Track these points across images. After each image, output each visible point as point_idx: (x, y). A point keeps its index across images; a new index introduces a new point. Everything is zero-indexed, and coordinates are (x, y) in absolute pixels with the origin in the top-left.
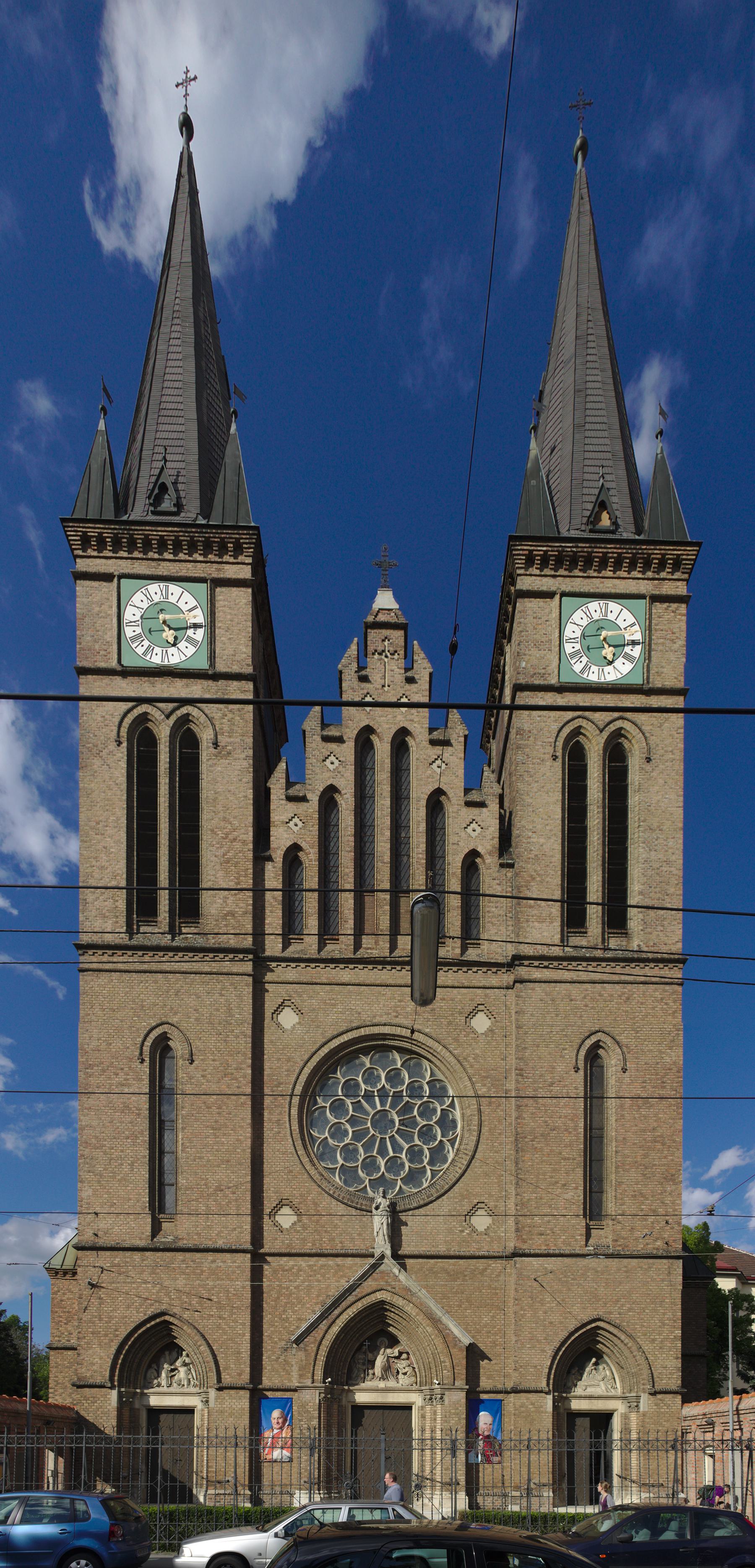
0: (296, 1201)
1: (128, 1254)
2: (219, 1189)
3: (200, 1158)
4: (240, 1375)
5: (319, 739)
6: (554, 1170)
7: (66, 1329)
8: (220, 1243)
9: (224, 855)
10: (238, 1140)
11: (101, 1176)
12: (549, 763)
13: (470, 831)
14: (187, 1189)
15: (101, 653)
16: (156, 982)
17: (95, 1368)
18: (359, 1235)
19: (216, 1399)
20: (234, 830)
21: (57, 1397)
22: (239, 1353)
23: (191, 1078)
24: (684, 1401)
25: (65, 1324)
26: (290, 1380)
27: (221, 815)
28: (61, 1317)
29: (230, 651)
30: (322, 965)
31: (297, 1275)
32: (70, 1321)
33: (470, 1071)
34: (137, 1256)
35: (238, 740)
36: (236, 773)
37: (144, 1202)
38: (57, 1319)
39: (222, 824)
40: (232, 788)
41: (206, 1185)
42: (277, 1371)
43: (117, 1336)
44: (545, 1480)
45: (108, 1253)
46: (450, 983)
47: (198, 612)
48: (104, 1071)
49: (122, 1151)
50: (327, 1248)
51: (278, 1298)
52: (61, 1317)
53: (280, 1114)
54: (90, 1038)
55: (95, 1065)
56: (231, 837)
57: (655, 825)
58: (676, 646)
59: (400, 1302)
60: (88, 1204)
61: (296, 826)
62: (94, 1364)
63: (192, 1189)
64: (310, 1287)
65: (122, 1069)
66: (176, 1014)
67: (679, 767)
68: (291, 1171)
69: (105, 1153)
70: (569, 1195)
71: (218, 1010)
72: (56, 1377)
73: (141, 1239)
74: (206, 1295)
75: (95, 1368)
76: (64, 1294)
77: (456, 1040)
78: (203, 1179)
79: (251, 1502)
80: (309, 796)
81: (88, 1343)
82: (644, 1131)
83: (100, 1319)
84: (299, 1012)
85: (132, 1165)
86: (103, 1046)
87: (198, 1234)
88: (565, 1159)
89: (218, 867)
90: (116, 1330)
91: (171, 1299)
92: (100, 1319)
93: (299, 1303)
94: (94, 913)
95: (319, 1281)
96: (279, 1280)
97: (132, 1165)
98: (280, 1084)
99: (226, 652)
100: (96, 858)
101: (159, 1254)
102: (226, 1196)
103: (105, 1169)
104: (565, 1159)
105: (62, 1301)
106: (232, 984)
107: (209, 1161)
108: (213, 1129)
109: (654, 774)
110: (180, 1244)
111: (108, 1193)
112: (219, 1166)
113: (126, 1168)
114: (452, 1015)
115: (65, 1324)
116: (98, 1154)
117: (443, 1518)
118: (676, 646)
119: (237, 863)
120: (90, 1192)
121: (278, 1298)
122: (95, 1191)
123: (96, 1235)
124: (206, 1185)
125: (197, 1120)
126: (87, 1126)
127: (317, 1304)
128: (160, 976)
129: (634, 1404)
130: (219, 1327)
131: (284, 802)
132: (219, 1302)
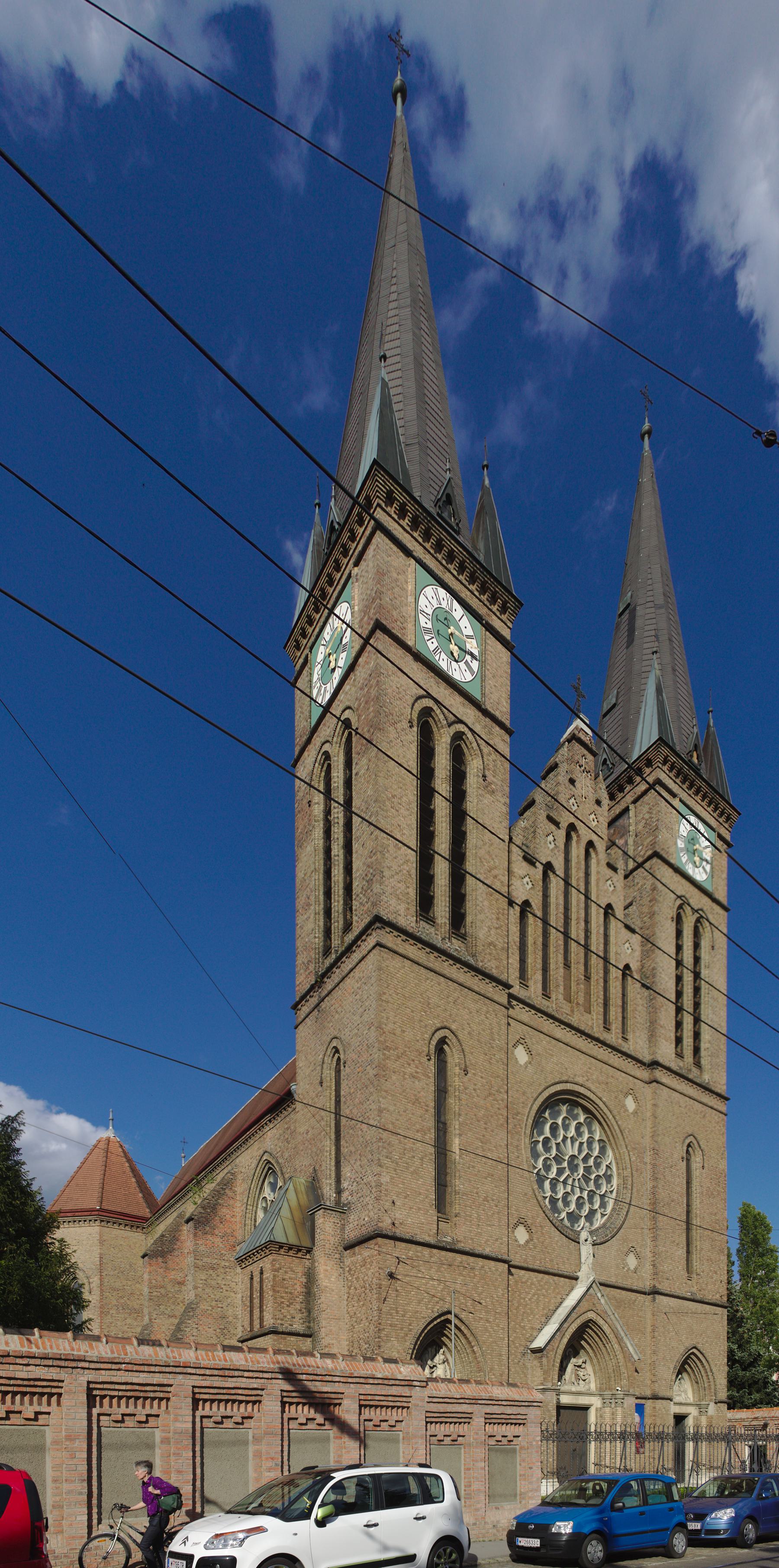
0: (529, 1222)
1: (420, 1248)
3: (473, 1167)
5: (544, 815)
7: (289, 1312)
8: (487, 1251)
11: (397, 1163)
14: (464, 1194)
15: (398, 623)
20: (496, 868)
22: (501, 1355)
23: (466, 1089)
24: (729, 1408)
25: (288, 1306)
28: (282, 1297)
30: (545, 1018)
32: (292, 1304)
34: (426, 1251)
38: (279, 1300)
39: (487, 857)
43: (410, 1330)
44: (670, 1466)
45: (403, 1245)
48: (399, 1057)
50: (549, 1267)
51: (518, 1307)
52: (282, 1297)
55: (390, 1048)
59: (601, 1322)
60: (386, 1190)
63: (466, 1194)
65: (413, 1060)
66: (454, 1021)
67: (725, 961)
68: (526, 1194)
71: (484, 1030)
73: (429, 1236)
74: (477, 1299)
76: (286, 1272)
77: (619, 1113)
78: (474, 1188)
79: (144, 1502)
83: (397, 1312)
84: (529, 1052)
85: (422, 1159)
86: (398, 1031)
87: (472, 1239)
89: (484, 896)
90: (410, 1325)
92: (397, 1312)
93: (532, 1313)
98: (519, 1113)
101: (444, 1253)
102: (491, 1207)
106: (494, 1011)
107: (479, 1171)
108: (482, 1142)
109: (715, 959)
110: (460, 1246)
111: (403, 1183)
113: (417, 1162)
115: (288, 1306)
120: (388, 1179)
121: (518, 1307)
122: (392, 1178)
123: (394, 1224)
126: (385, 1109)
128: (442, 979)
129: (702, 1409)
130: (486, 1330)
131: (521, 859)
132: (486, 1306)
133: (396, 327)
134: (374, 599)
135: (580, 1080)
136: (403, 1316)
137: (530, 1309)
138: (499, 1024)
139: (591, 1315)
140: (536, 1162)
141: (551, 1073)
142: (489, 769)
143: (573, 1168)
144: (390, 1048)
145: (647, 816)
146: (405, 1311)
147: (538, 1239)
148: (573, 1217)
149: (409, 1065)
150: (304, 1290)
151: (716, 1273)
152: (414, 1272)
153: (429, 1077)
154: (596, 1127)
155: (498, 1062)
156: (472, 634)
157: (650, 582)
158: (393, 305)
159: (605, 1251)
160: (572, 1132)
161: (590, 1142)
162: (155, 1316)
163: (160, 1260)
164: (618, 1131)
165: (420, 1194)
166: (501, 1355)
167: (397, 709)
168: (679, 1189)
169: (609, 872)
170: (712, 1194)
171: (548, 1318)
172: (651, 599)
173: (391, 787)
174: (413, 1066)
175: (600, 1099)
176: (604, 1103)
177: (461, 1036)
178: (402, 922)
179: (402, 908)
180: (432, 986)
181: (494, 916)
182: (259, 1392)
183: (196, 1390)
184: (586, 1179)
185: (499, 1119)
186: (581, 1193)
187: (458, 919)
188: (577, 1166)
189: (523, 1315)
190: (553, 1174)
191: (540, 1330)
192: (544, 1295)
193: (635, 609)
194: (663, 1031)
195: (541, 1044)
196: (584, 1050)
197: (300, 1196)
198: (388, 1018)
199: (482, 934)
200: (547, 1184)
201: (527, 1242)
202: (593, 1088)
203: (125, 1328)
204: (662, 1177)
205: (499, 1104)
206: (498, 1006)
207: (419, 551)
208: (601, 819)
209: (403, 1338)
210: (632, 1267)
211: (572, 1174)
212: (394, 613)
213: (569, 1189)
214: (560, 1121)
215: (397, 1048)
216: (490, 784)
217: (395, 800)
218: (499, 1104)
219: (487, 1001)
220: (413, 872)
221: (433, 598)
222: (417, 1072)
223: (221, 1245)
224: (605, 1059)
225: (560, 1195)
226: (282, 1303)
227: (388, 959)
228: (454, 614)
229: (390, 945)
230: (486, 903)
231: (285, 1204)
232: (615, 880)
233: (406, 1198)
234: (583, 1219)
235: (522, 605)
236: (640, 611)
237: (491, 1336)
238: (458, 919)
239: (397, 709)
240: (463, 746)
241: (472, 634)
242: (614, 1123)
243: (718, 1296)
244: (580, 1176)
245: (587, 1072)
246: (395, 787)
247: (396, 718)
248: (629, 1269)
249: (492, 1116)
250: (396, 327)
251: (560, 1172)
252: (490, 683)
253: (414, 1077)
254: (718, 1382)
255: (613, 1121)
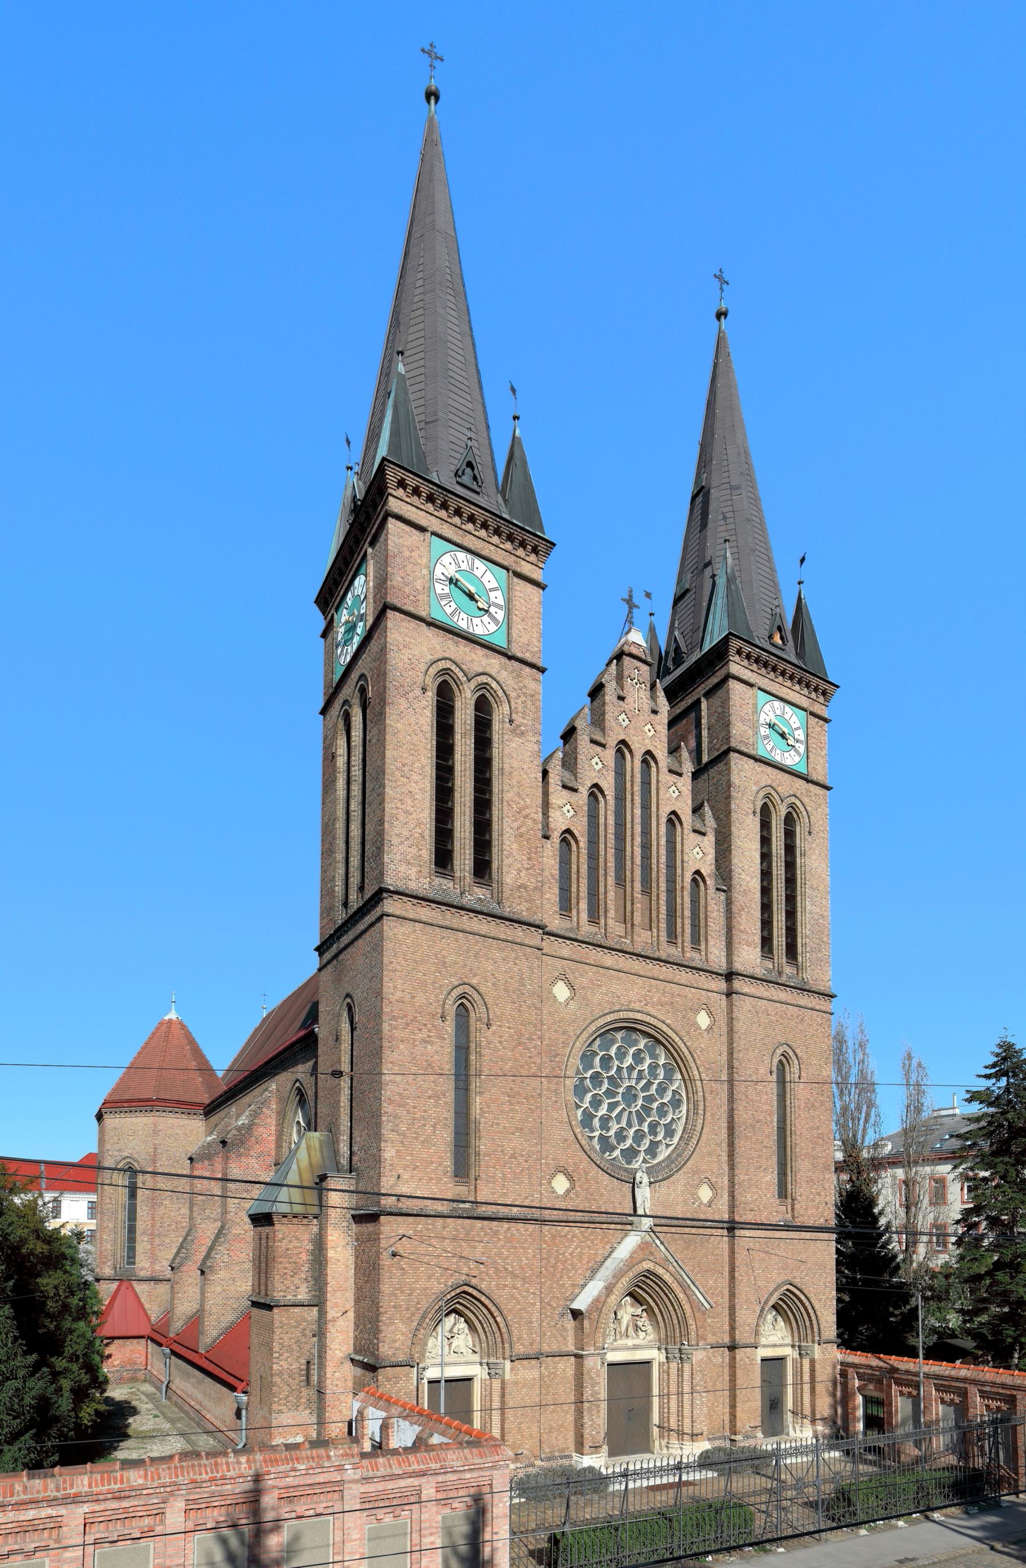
0: (570, 1169)
2: (513, 1156)
3: (497, 1124)
4: (531, 1344)
5: (587, 739)
6: (759, 1156)
7: (292, 1282)
9: (518, 828)
10: (530, 1109)
11: (404, 1135)
12: (751, 817)
13: (698, 853)
14: (485, 1155)
15: (411, 597)
16: (457, 940)
17: (397, 1345)
18: (620, 1203)
19: (512, 1370)
20: (527, 807)
21: (281, 1363)
22: (531, 1322)
26: (567, 1346)
27: (516, 789)
28: (285, 1268)
29: (524, 640)
31: (572, 1241)
32: (296, 1274)
33: (698, 1062)
35: (530, 723)
36: (529, 754)
37: (446, 1167)
39: (517, 798)
40: (524, 767)
41: (502, 1151)
42: (556, 1337)
43: (419, 1309)
46: (683, 982)
47: (499, 594)
48: (407, 1024)
49: (425, 1111)
52: (285, 1268)
53: (557, 1084)
54: (395, 987)
55: (398, 1018)
56: (524, 813)
57: (815, 886)
58: (823, 753)
60: (391, 1165)
61: (568, 811)
62: (396, 1341)
64: (581, 1255)
65: (425, 1025)
66: (475, 976)
68: (566, 1140)
69: (408, 1112)
70: (768, 1178)
71: (512, 978)
72: (282, 1339)
75: (397, 1345)
76: (290, 1242)
77: (688, 1033)
80: (581, 789)
81: (389, 1318)
82: (812, 1128)
84: (571, 987)
88: (766, 1147)
89: (513, 839)
90: (418, 1303)
91: (470, 1269)
93: (573, 1269)
94: (398, 857)
95: (588, 1247)
96: (557, 1246)
97: (434, 1126)
99: (521, 639)
100: (401, 800)
102: (519, 1164)
103: (408, 1129)
104: (766, 1147)
105: (287, 1249)
107: (505, 1128)
108: (509, 1096)
109: (814, 845)
111: (411, 1155)
112: (513, 1134)
113: (429, 1129)
114: (685, 1010)
115: (292, 1276)
116: (401, 1112)
117: (14, 1318)
118: (823, 753)
119: (529, 839)
122: (398, 1151)
124: (502, 1151)
125: (494, 1086)
127: (587, 1270)
128: (461, 934)
130: (513, 1297)
131: (560, 788)
133: (421, 311)
134: (382, 583)
135: (636, 1006)
136: (410, 1295)
137: (571, 1265)
138: (531, 968)
139: (647, 1265)
140: (582, 1100)
141: (600, 1004)
142: (517, 713)
143: (630, 1096)
144: (398, 1018)
145: (720, 710)
146: (413, 1290)
147: (581, 1187)
148: (630, 1154)
149: (420, 1030)
150: (310, 1257)
151: (819, 1194)
152: (422, 1248)
153: (445, 1039)
154: (660, 1051)
155: (529, 1008)
156: (497, 585)
157: (725, 463)
158: (417, 291)
159: (669, 1188)
160: (629, 1061)
161: (653, 1068)
162: (199, 1221)
163: (206, 1163)
164: (687, 1053)
165: (432, 1162)
166: (531, 1322)
167: (408, 680)
168: (766, 1107)
169: (674, 778)
170: (813, 1105)
171: (594, 1271)
172: (727, 480)
173: (401, 757)
174: (425, 1031)
175: (663, 1022)
176: (668, 1026)
177: (482, 989)
178: (413, 886)
179: (413, 872)
180: (449, 946)
181: (525, 858)
182: (162, 1505)
183: (87, 1516)
184: (647, 1110)
185: (531, 1068)
186: (640, 1125)
187: (482, 868)
188: (635, 1096)
189: (561, 1272)
190: (603, 1110)
191: (584, 1286)
192: (588, 1247)
193: (708, 492)
194: (744, 937)
195: (584, 977)
196: (642, 973)
197: (313, 1153)
198: (395, 987)
199: (509, 879)
200: (596, 1122)
201: (568, 1191)
202: (653, 1012)
203: (179, 1218)
204: (743, 1097)
205: (531, 1052)
206: (529, 950)
207: (434, 524)
208: (659, 728)
209: (408, 1318)
210: (705, 1200)
211: (629, 1106)
212: (407, 590)
213: (624, 1124)
214: (613, 1052)
215: (405, 1016)
216: (518, 726)
217: (406, 769)
218: (531, 1052)
219: (516, 947)
220: (427, 833)
221: (450, 563)
222: (429, 1036)
223: (256, 1166)
224: (670, 977)
225: (612, 1133)
226: (286, 1274)
227: (395, 927)
228: (476, 572)
229: (397, 912)
230: (515, 846)
231: (294, 1166)
232: (679, 785)
233: (414, 1169)
234: (643, 1154)
235: (554, 545)
236: (714, 494)
237: (518, 1303)
238: (482, 868)
239: (408, 680)
240: (488, 695)
241: (497, 585)
242: (682, 1046)
243: (822, 1221)
244: (638, 1108)
245: (646, 996)
246: (405, 755)
247: (407, 689)
248: (701, 1203)
249: (522, 1067)
250: (421, 311)
251: (612, 1107)
252: (518, 627)
253: (425, 1042)
254: (822, 1321)
255: (680, 1043)
